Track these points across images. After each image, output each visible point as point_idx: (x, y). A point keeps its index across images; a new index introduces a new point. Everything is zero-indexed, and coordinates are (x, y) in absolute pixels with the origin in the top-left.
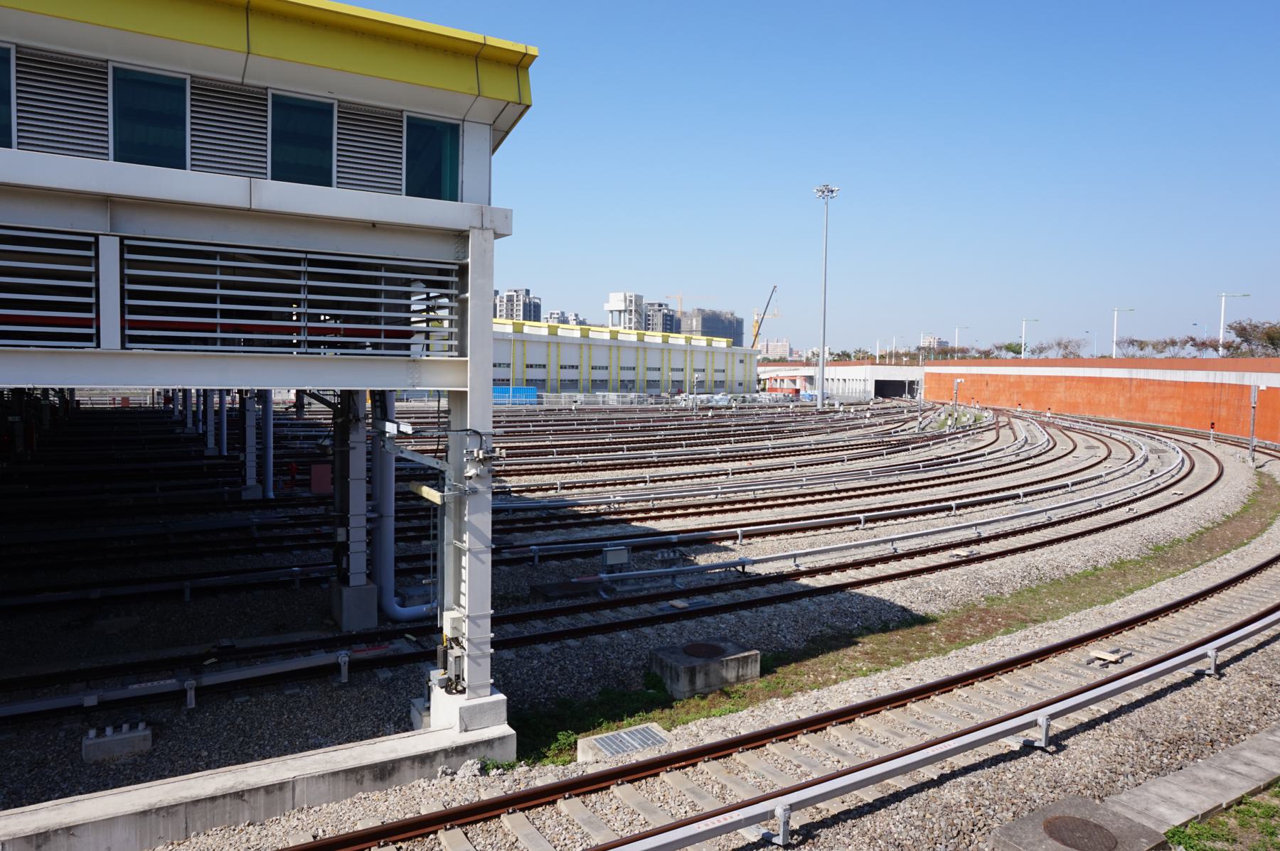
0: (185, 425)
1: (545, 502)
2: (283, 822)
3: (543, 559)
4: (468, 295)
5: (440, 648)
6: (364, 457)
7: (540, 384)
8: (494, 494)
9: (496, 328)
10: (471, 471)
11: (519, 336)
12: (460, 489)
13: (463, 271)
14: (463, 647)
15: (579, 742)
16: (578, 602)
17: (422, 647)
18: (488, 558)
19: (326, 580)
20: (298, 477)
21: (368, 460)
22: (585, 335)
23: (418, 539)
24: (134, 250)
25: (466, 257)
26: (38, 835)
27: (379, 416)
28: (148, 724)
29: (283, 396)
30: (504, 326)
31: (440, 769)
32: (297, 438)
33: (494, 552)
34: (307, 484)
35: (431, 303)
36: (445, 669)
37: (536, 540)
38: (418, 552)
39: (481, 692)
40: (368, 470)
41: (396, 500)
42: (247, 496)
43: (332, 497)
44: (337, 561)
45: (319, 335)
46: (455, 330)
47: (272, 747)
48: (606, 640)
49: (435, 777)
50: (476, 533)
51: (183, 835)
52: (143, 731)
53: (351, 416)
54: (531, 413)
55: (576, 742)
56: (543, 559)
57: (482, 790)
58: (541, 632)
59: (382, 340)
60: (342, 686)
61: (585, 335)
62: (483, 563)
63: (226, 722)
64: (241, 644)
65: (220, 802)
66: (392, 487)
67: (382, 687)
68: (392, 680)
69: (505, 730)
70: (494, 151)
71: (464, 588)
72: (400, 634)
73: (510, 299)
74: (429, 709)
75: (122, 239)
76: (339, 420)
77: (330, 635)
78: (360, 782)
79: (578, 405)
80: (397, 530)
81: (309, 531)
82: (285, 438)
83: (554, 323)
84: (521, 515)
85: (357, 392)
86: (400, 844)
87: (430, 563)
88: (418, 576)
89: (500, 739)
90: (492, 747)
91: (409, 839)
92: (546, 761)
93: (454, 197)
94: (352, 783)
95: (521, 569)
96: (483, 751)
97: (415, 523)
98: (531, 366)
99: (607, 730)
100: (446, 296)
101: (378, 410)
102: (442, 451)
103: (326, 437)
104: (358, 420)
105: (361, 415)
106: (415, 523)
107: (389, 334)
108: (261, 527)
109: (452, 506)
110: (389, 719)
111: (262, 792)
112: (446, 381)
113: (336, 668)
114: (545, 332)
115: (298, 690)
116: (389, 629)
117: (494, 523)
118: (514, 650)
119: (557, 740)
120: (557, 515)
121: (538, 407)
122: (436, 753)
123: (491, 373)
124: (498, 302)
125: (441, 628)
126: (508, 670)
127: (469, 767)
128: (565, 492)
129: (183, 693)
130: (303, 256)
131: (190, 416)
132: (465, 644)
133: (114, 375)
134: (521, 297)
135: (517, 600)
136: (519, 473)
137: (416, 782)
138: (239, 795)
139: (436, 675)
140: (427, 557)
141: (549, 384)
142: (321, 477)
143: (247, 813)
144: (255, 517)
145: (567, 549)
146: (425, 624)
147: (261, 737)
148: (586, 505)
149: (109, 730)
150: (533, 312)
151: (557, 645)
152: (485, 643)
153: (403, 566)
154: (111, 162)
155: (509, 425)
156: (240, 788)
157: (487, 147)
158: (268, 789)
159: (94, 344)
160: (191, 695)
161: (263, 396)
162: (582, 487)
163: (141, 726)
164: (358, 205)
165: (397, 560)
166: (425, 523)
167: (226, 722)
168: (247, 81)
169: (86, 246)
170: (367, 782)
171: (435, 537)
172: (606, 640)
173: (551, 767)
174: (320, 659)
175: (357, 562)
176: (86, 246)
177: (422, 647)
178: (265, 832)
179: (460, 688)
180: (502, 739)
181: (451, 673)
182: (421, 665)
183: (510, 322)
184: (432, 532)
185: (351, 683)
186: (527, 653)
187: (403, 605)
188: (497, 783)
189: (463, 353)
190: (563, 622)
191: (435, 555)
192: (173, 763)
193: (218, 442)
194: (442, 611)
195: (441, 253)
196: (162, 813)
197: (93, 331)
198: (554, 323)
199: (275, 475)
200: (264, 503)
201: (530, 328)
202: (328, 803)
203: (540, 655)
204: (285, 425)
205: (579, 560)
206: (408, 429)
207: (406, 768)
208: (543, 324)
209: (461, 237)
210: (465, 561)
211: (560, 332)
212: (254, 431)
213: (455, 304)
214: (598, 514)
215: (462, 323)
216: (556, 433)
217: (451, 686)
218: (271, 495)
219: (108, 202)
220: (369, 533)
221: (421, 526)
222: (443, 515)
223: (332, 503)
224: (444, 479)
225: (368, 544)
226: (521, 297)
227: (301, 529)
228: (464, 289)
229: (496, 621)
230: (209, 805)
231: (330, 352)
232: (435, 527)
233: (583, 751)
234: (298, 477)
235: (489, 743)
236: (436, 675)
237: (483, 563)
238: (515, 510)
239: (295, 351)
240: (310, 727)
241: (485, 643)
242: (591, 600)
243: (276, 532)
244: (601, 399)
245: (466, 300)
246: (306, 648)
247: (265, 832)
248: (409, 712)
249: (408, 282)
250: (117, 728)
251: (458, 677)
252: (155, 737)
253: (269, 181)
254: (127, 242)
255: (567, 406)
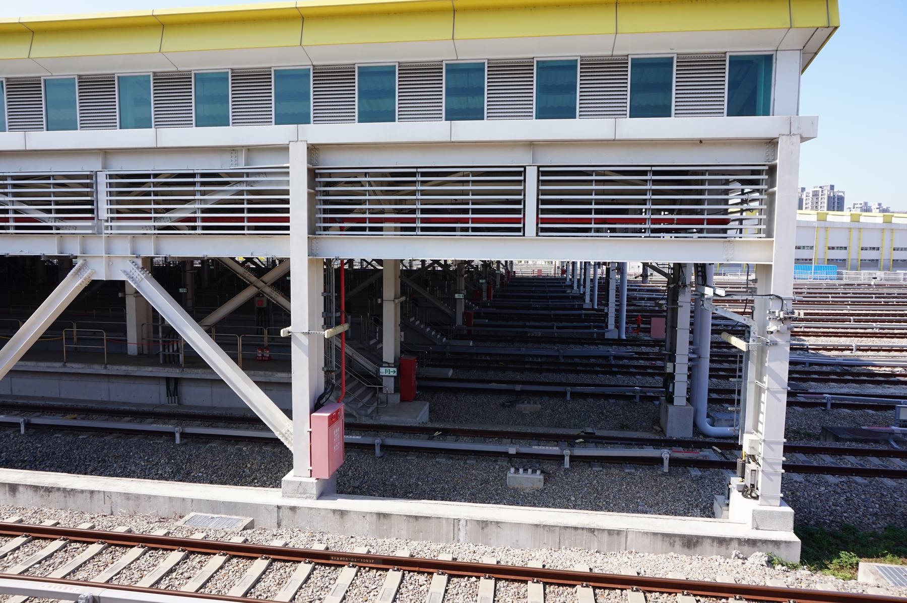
0: (573, 288)
1: (840, 360)
2: (618, 557)
3: (834, 406)
4: (776, 189)
5: (739, 461)
6: (689, 314)
7: (842, 263)
8: (791, 349)
9: (799, 218)
10: (772, 327)
11: (823, 224)
12: (762, 341)
13: (772, 170)
14: (758, 464)
15: (861, 564)
16: (867, 447)
17: (726, 458)
18: (784, 398)
19: (657, 398)
20: (642, 326)
21: (691, 317)
22: (888, 221)
23: (726, 378)
24: (545, 173)
25: (774, 159)
26: (483, 521)
27: (700, 282)
28: (542, 472)
29: (634, 269)
30: (809, 216)
31: (734, 552)
32: (643, 299)
33: (789, 394)
34: (648, 331)
35: (744, 197)
36: (743, 477)
37: (830, 390)
38: (727, 387)
39: (772, 502)
40: (691, 324)
41: (711, 347)
42: (608, 336)
43: (664, 341)
44: (666, 386)
45: (570, 219)
46: (764, 217)
47: (614, 505)
48: (895, 484)
49: (730, 558)
50: (775, 377)
51: (557, 546)
52: (539, 476)
53: (680, 283)
54: (829, 287)
55: (857, 564)
56: (834, 406)
57: (767, 578)
58: (829, 465)
59: (705, 226)
60: (664, 474)
61: (888, 221)
62: (779, 400)
63: (587, 482)
64: (599, 433)
65: (580, 531)
66: (708, 338)
67: (693, 481)
68: (701, 478)
69: (790, 536)
70: (803, 71)
71: (762, 418)
72: (709, 445)
73: (815, 194)
74: (728, 505)
75: (539, 167)
76: (672, 286)
77: (657, 437)
78: (672, 545)
79: (877, 281)
80: (711, 369)
81: (648, 363)
82: (635, 298)
83: (858, 212)
84: (817, 368)
85: (685, 264)
86: (698, 598)
87: (736, 397)
88: (726, 405)
89: (786, 542)
90: (779, 548)
91: (707, 596)
92: (826, 571)
93: (766, 113)
94: (667, 544)
95: (814, 411)
96: (770, 549)
97: (726, 366)
98: (833, 248)
99: (891, 562)
100: (758, 190)
101: (700, 278)
102: (749, 313)
103: (663, 299)
104: (685, 286)
105: (688, 283)
106: (726, 366)
107: (710, 222)
108: (616, 357)
109: (755, 353)
110: (697, 506)
111: (606, 532)
112: (755, 257)
113: (660, 461)
114: (847, 219)
115: (633, 471)
116: (700, 440)
117: (790, 372)
118: (803, 475)
119: (839, 557)
120: (849, 372)
121: (837, 282)
122: (731, 539)
123: (794, 254)
124: (804, 197)
125: (741, 446)
126: (797, 490)
127: (758, 558)
128: (860, 353)
129: (562, 457)
130: (649, 168)
131: (576, 282)
132: (760, 461)
133: (534, 255)
134: (826, 192)
135: (809, 436)
136: (817, 335)
137: (714, 557)
138: (592, 531)
139: (735, 481)
140: (733, 392)
141: (849, 263)
142: (658, 327)
143: (596, 544)
144: (613, 351)
145: (862, 400)
146: (729, 441)
147: (607, 497)
148: (881, 366)
149: (521, 470)
150: (836, 203)
151: (844, 479)
152: (777, 464)
153: (714, 396)
154: (534, 120)
155: (806, 296)
156: (592, 526)
157: (797, 67)
158: (610, 532)
159: (521, 234)
160: (567, 459)
161: (621, 268)
162: (878, 350)
163: (538, 472)
164: (695, 130)
165: (710, 391)
166: (733, 366)
167: (587, 482)
168: (615, 53)
169: (518, 174)
170: (678, 545)
171: (740, 377)
172: (895, 484)
173: (832, 577)
174: (649, 452)
175: (680, 388)
176: (518, 174)
177: (726, 458)
178: (606, 560)
179: (754, 495)
180: (788, 543)
181: (748, 481)
182: (724, 471)
183: (815, 212)
184: (738, 374)
185: (670, 473)
186: (815, 480)
187: (713, 425)
188: (781, 576)
189: (769, 234)
190: (851, 461)
191: (739, 391)
192: (554, 499)
193: (592, 300)
194: (743, 432)
195: (755, 158)
196: (546, 529)
197: (521, 226)
198: (858, 212)
199: (627, 323)
200: (619, 342)
201: (833, 217)
202: (649, 553)
203: (827, 484)
204: (635, 290)
205: (871, 412)
206: (721, 292)
207: (707, 543)
208: (846, 212)
209: (772, 143)
210: (764, 397)
211: (862, 219)
212: (614, 293)
213: (764, 197)
214: (893, 375)
215: (770, 212)
216: (853, 304)
217: (748, 491)
218: (624, 337)
219: (531, 145)
220: (690, 369)
221: (728, 368)
222: (748, 359)
223: (664, 346)
224: (749, 332)
225: (689, 377)
226: (826, 192)
227: (642, 362)
228: (772, 184)
229: (787, 449)
230: (573, 531)
231: (667, 236)
232: (741, 370)
233: (865, 573)
234: (642, 326)
235: (776, 543)
236: (735, 481)
237: (779, 400)
238: (811, 364)
239: (643, 235)
240: (640, 497)
241: (777, 464)
242: (881, 447)
243: (626, 362)
244: (902, 277)
245: (774, 194)
246: (641, 443)
247: (606, 560)
248: (712, 504)
249: (727, 182)
250: (525, 470)
251: (753, 486)
252: (546, 481)
253: (628, 119)
254: (541, 169)
255: (866, 282)
